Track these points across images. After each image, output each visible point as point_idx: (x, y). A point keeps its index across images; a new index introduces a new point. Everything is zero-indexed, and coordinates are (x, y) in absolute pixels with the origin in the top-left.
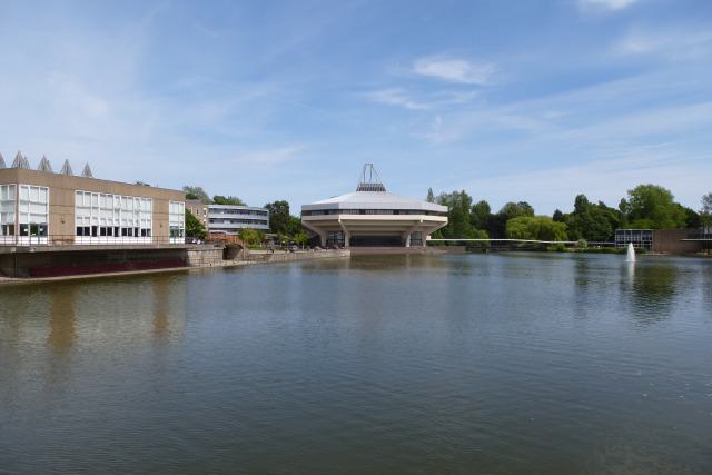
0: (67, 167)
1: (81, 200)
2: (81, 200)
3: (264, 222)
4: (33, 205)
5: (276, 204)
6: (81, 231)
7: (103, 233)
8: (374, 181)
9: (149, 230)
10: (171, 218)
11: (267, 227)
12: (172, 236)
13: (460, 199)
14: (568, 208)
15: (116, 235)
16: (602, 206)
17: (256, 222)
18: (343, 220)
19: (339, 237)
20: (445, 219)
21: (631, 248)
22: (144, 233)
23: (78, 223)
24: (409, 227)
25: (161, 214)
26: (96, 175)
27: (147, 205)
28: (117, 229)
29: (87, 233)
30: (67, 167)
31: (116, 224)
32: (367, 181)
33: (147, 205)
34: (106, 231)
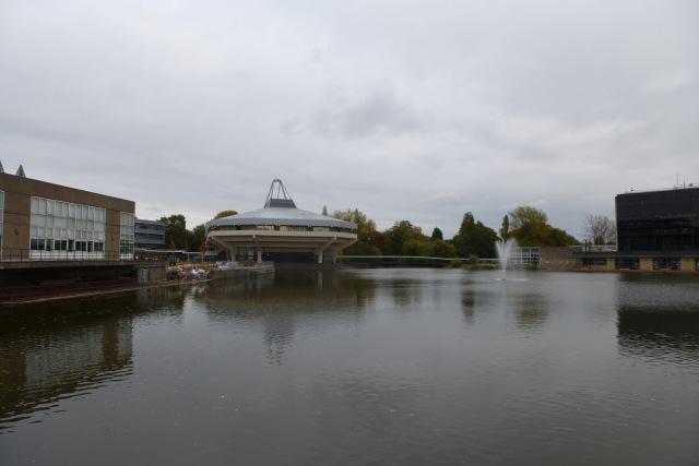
0: (438, 233)
1: (37, 206)
2: (37, 206)
3: (159, 237)
4: (687, 265)
5: (174, 218)
6: (38, 245)
7: (57, 248)
8: (282, 197)
9: (101, 244)
10: (123, 231)
11: (160, 242)
12: (122, 251)
13: (646, 265)
14: (428, 232)
15: (89, 250)
16: (419, 230)
17: (152, 236)
18: (257, 236)
19: (251, 253)
20: (355, 236)
21: (320, 261)
22: (98, 247)
23: (33, 236)
24: (322, 244)
25: (112, 226)
26: (29, 175)
27: (98, 215)
28: (90, 243)
29: (41, 248)
30: (438, 233)
31: (47, 236)
32: (275, 197)
33: (98, 215)
34: (81, 246)
